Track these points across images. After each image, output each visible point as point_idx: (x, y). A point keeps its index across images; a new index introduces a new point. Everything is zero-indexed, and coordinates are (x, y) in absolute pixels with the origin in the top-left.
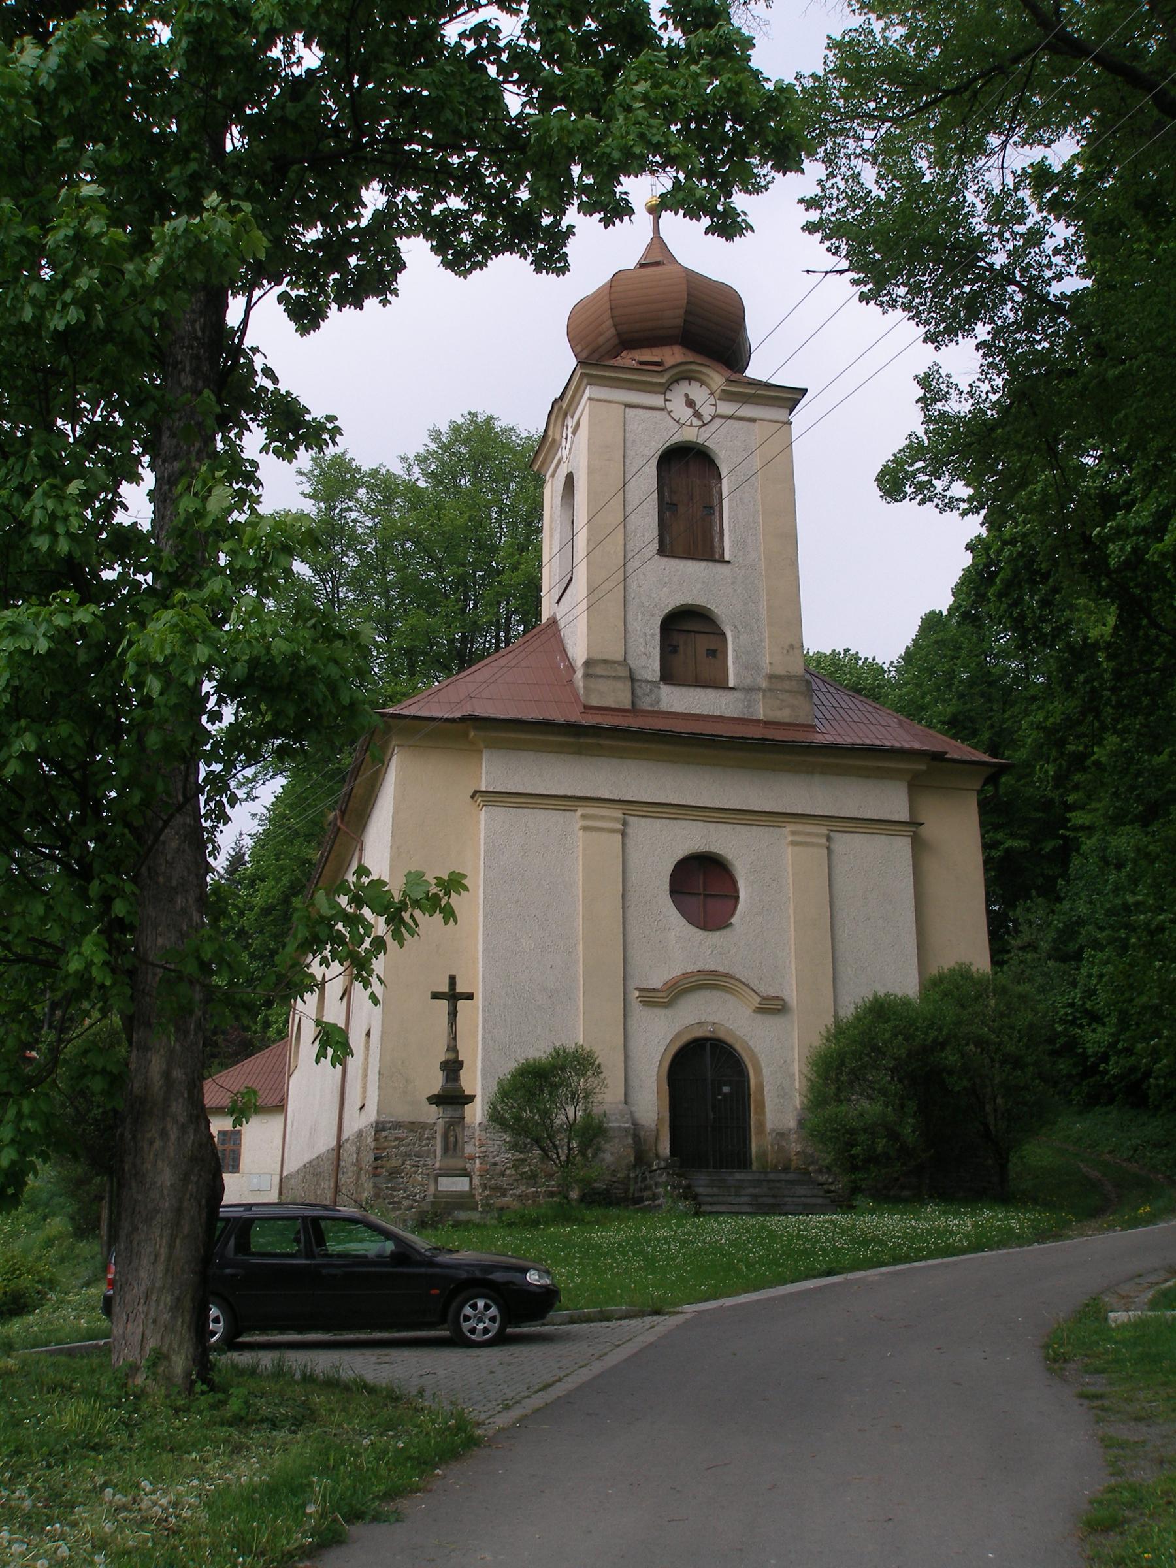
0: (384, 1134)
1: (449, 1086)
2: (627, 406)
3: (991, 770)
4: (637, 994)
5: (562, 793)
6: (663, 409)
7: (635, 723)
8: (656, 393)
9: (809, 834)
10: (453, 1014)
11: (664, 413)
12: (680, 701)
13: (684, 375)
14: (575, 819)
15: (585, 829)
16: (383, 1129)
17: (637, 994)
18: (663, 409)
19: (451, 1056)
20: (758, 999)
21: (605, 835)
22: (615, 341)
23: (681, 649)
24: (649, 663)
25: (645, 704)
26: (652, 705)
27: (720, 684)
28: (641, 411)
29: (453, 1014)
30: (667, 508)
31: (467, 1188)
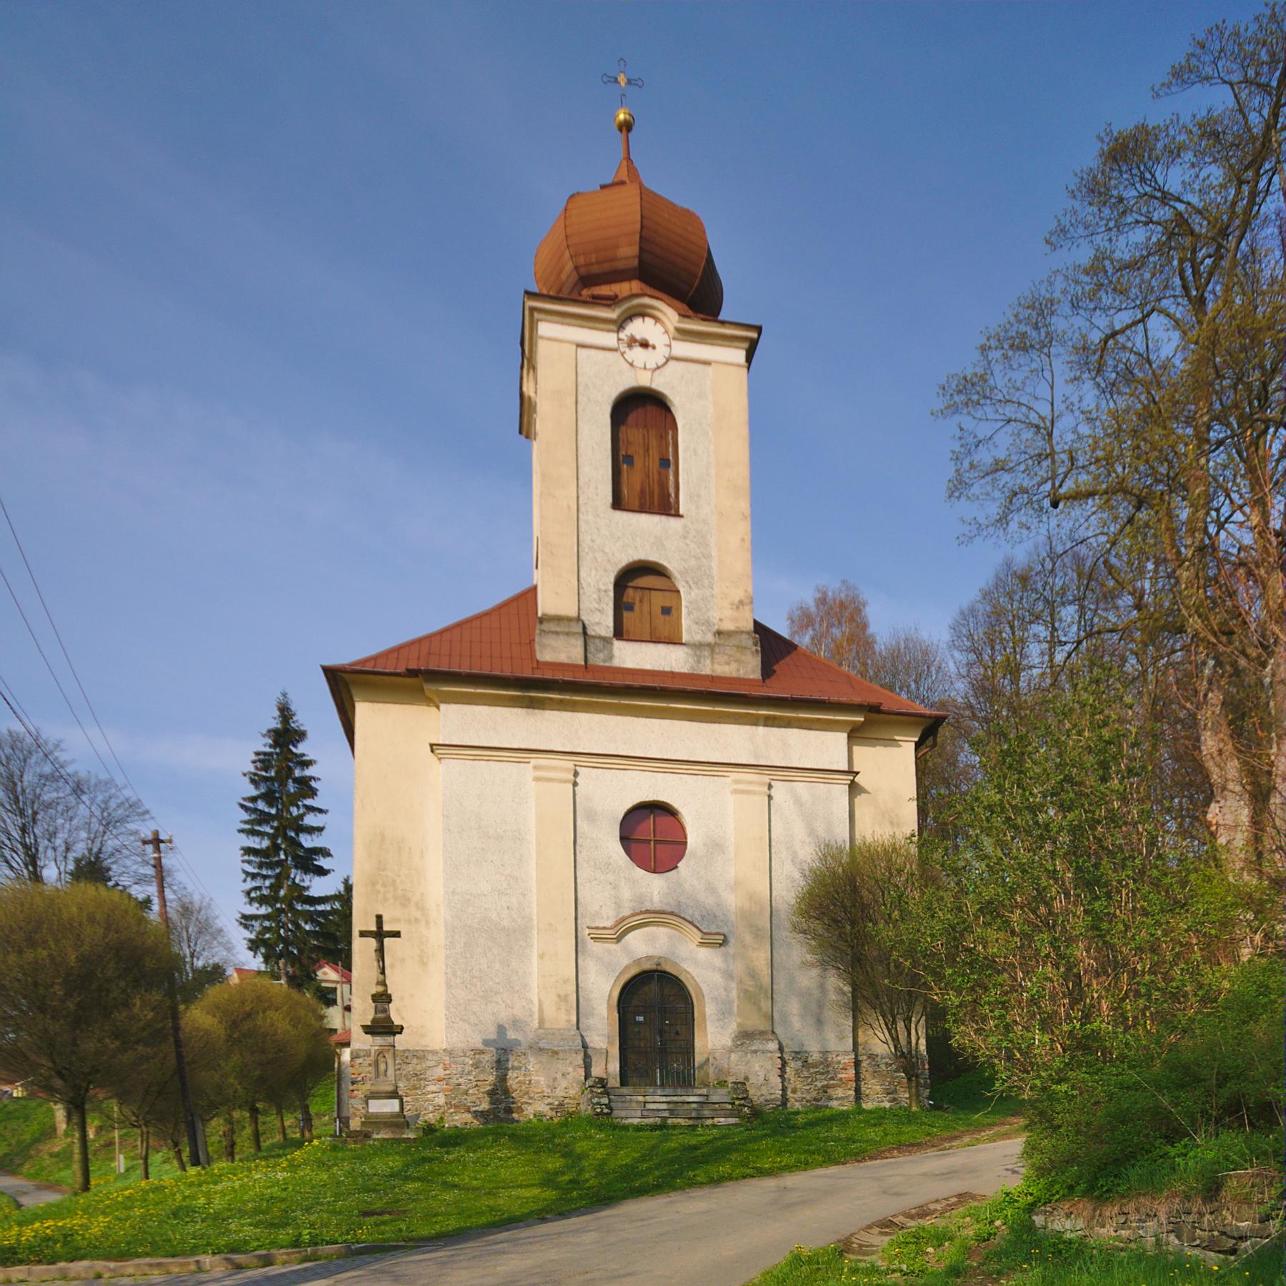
0: (359, 1061)
1: (380, 1015)
2: (579, 345)
3: (929, 722)
4: (588, 931)
5: (516, 746)
6: (616, 350)
7: (589, 679)
8: (609, 331)
9: (751, 783)
10: (380, 951)
11: (617, 355)
12: (635, 657)
13: (638, 310)
14: (526, 771)
15: (537, 779)
16: (358, 1057)
17: (588, 931)
18: (616, 350)
19: (381, 989)
20: (700, 935)
21: (556, 785)
22: (575, 277)
23: (637, 607)
24: (603, 622)
25: (598, 659)
26: (604, 661)
27: (674, 640)
28: (593, 352)
29: (380, 951)
30: (620, 460)
31: (397, 1109)
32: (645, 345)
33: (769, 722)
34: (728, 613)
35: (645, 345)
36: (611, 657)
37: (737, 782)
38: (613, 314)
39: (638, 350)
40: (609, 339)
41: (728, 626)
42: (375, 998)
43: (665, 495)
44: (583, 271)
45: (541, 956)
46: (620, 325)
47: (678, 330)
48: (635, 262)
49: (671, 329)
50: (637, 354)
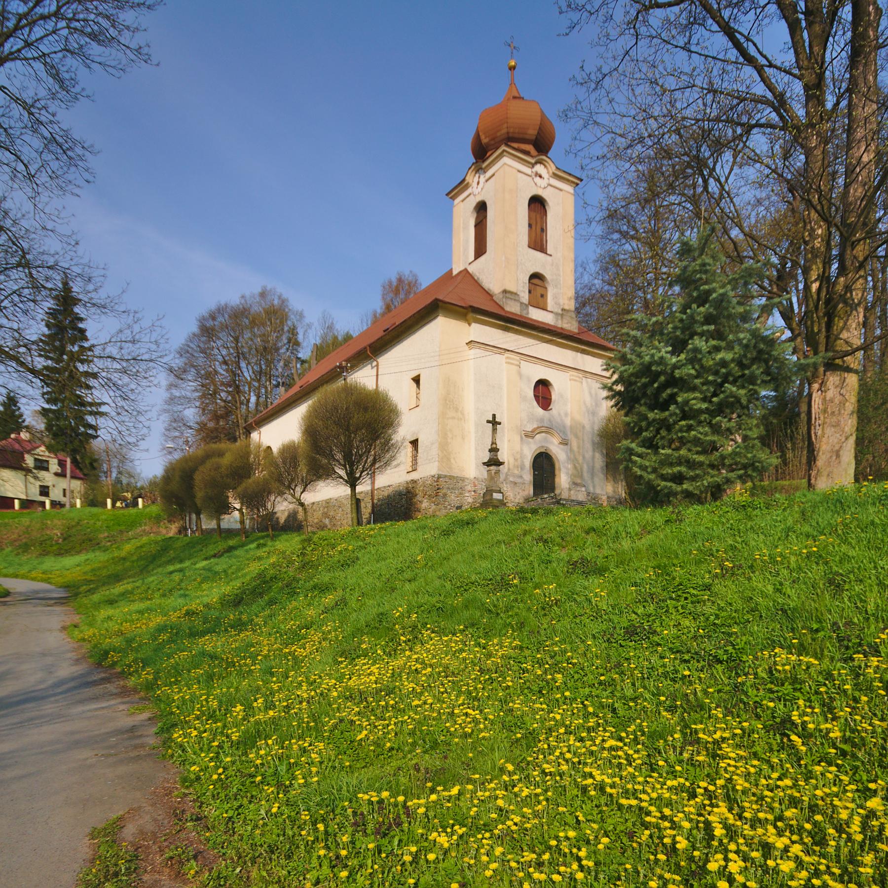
11: (529, 179)
24: (525, 297)
32: (540, 177)
33: (583, 352)
34: (566, 302)
35: (540, 177)
36: (528, 313)
37: (507, 358)
38: (533, 161)
39: (538, 178)
40: (528, 170)
41: (566, 307)
42: (488, 464)
43: (542, 245)
44: (511, 135)
45: (509, 441)
46: (533, 165)
47: (554, 174)
48: (534, 138)
49: (551, 172)
50: (537, 179)
